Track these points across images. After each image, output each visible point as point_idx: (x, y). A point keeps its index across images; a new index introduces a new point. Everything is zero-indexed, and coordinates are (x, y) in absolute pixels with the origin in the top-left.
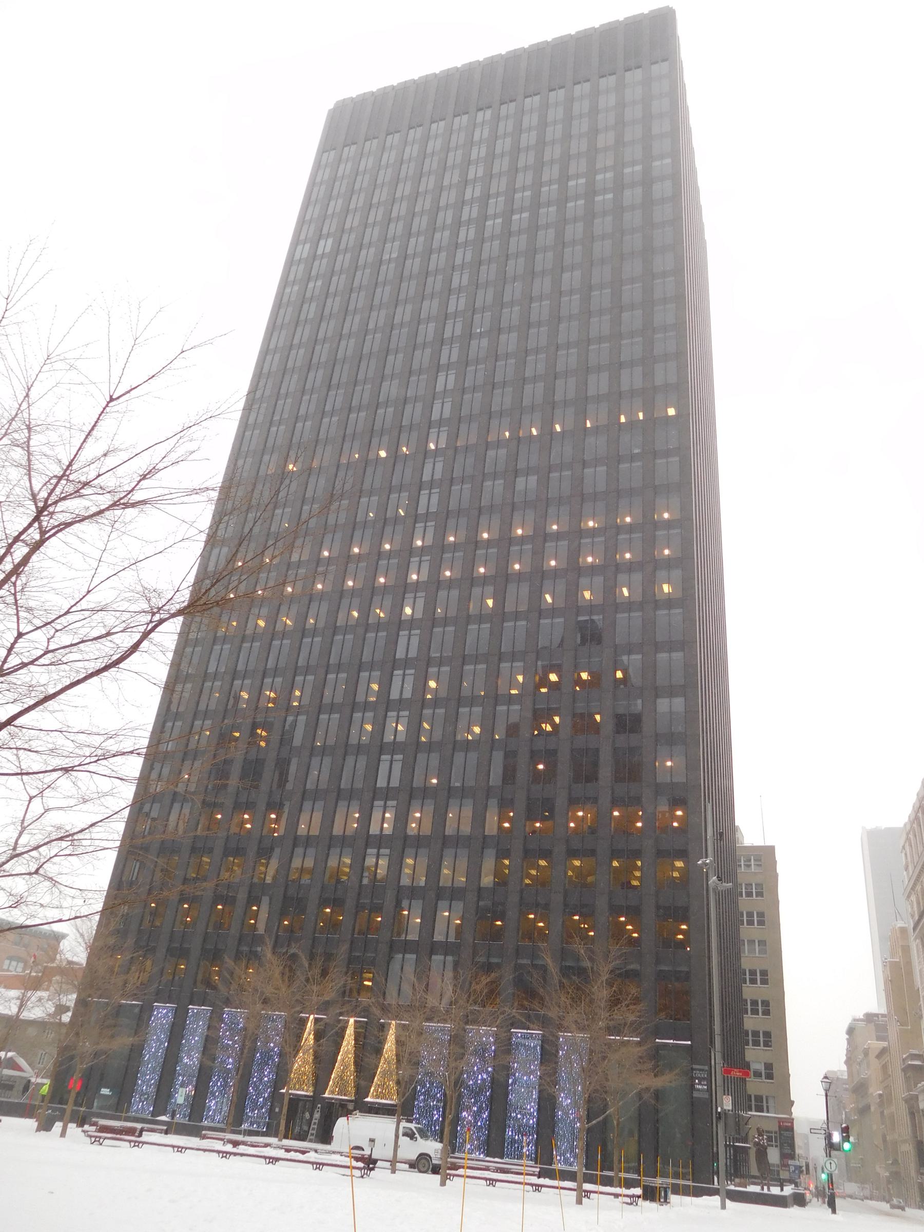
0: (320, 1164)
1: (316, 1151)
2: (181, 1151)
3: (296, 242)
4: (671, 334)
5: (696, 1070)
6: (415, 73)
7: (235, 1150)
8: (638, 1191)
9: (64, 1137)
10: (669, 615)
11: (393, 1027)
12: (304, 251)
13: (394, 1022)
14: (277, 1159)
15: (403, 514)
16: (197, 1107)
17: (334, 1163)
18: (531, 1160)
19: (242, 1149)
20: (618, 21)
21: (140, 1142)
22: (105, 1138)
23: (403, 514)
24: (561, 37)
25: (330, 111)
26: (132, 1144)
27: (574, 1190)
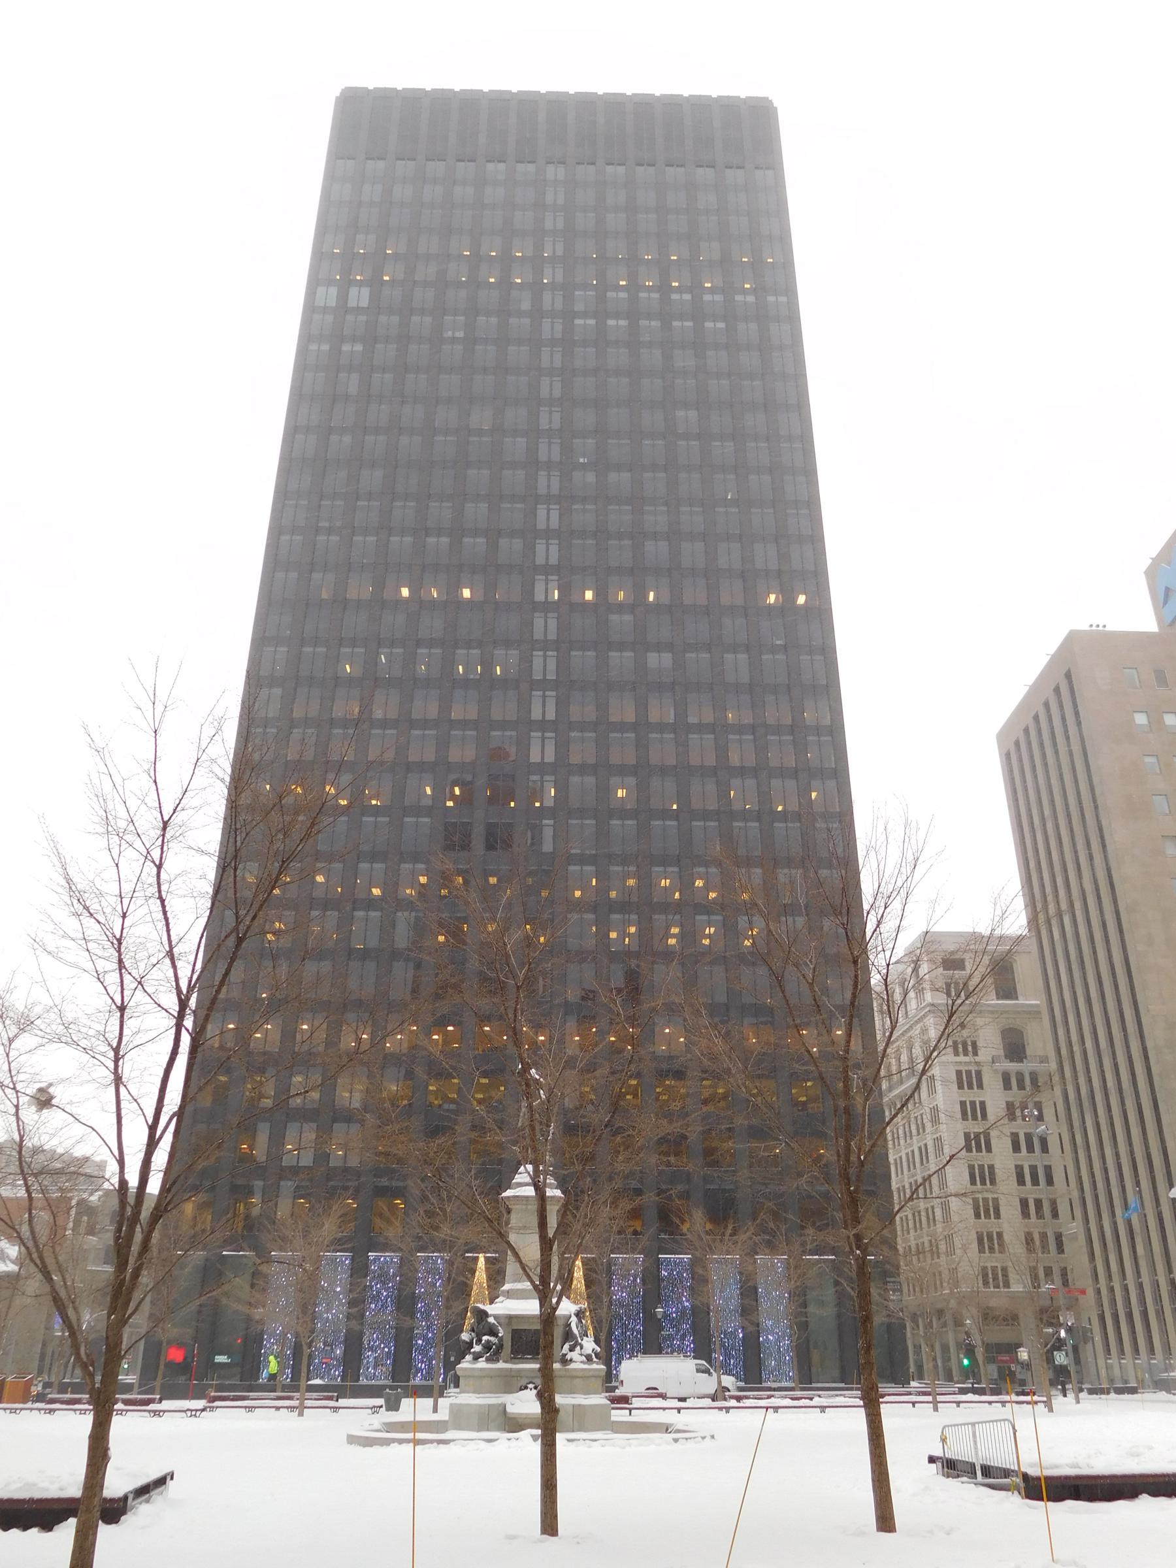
0: (336, 1408)
1: (819, 1396)
2: (195, 1415)
3: (314, 282)
4: (412, 504)
5: (889, 1282)
6: (429, 83)
7: (741, 1404)
8: (380, 1401)
9: (303, 1415)
10: (623, 826)
11: (578, 1263)
12: (329, 296)
13: (481, 1255)
14: (54, 1410)
15: (499, 673)
16: (352, 1361)
17: (834, 1405)
18: (741, 1381)
19: (748, 1403)
20: (510, 92)
21: (213, 1407)
22: (21, 1409)
23: (499, 673)
24: (385, 89)
25: (337, 98)
26: (152, 1415)
27: (931, 1402)
